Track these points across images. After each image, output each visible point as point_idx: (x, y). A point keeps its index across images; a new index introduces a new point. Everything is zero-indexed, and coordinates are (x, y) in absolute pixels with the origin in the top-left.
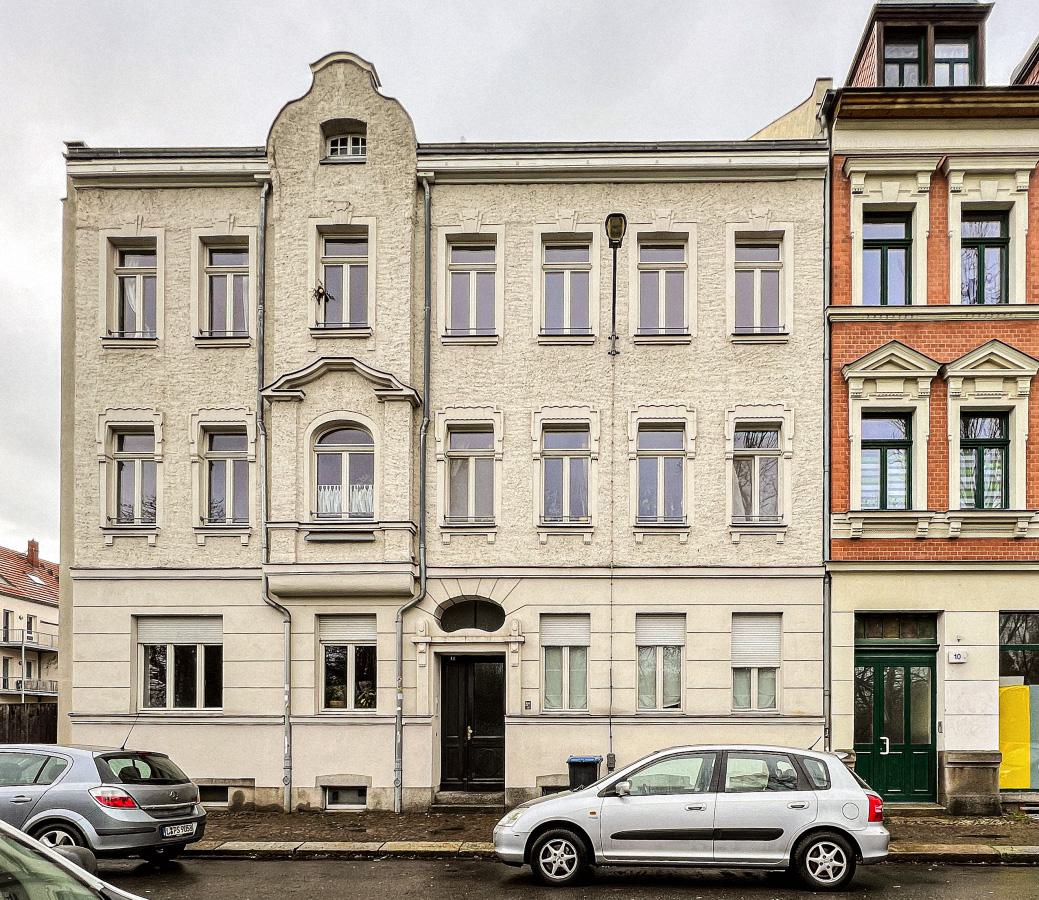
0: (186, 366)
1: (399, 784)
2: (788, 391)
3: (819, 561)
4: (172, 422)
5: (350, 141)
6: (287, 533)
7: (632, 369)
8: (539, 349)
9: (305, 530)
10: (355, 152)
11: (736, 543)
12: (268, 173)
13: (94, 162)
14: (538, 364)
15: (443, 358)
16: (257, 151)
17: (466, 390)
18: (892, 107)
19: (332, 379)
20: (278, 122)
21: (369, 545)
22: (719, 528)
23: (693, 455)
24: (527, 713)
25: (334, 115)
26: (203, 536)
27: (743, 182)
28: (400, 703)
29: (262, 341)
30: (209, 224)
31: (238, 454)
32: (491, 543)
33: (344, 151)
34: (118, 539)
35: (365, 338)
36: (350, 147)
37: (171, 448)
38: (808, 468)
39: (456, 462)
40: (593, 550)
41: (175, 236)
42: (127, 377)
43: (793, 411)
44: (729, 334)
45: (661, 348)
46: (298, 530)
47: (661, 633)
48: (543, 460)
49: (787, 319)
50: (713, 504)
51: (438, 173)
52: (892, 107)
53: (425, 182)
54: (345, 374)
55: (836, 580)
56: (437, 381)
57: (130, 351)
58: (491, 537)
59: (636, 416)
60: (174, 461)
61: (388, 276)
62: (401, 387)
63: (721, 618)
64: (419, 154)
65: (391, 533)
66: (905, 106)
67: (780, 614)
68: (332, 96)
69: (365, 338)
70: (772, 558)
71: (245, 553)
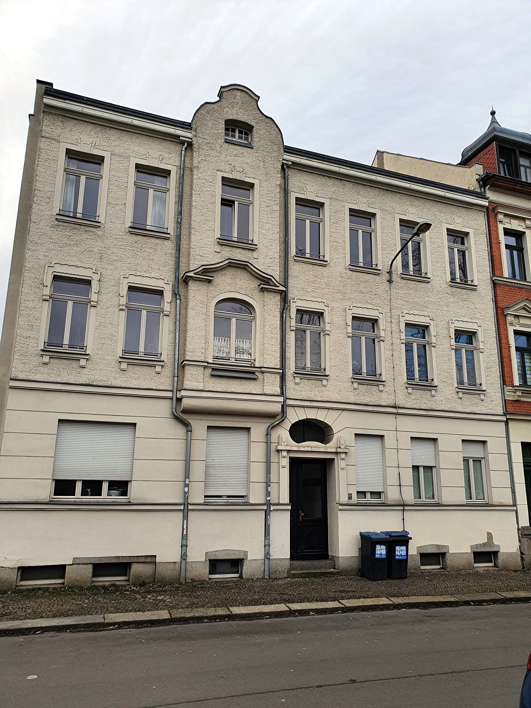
0: (119, 244)
1: (267, 556)
2: (478, 315)
3: (501, 412)
4: (106, 280)
5: (237, 132)
6: (198, 369)
7: (400, 291)
8: (350, 273)
9: (209, 367)
10: (240, 138)
11: (460, 398)
12: (191, 139)
13: (67, 101)
14: (349, 281)
15: (295, 269)
16: (183, 124)
17: (308, 290)
18: (514, 187)
19: (230, 273)
20: (199, 112)
21: (252, 382)
22: (451, 388)
23: (435, 345)
24: (351, 502)
25: (230, 118)
26: (411, 388)
27: (449, 204)
28: (268, 494)
29: (179, 238)
30: (144, 157)
31: (153, 307)
32: (325, 386)
33: (234, 136)
34: (53, 359)
35: (253, 250)
36: (237, 134)
37: (104, 298)
38: (492, 359)
39: (300, 333)
40: (384, 395)
41: (118, 159)
42: (72, 243)
43: (99, 274)
44: (347, 265)
45: (415, 282)
46: (205, 367)
47: (476, 452)
48: (51, 300)
49: (327, 252)
50: (447, 374)
51: (294, 163)
52: (514, 187)
53: (285, 166)
54: (239, 270)
55: (511, 424)
56: (292, 282)
57: (77, 226)
58: (325, 382)
59: (404, 319)
60: (105, 307)
61: (266, 216)
62: (278, 285)
63: (405, 441)
64: (284, 151)
65: (267, 374)
66: (520, 188)
67: (134, 425)
68: (233, 107)
69: (253, 250)
70: (479, 408)
71: (157, 378)
